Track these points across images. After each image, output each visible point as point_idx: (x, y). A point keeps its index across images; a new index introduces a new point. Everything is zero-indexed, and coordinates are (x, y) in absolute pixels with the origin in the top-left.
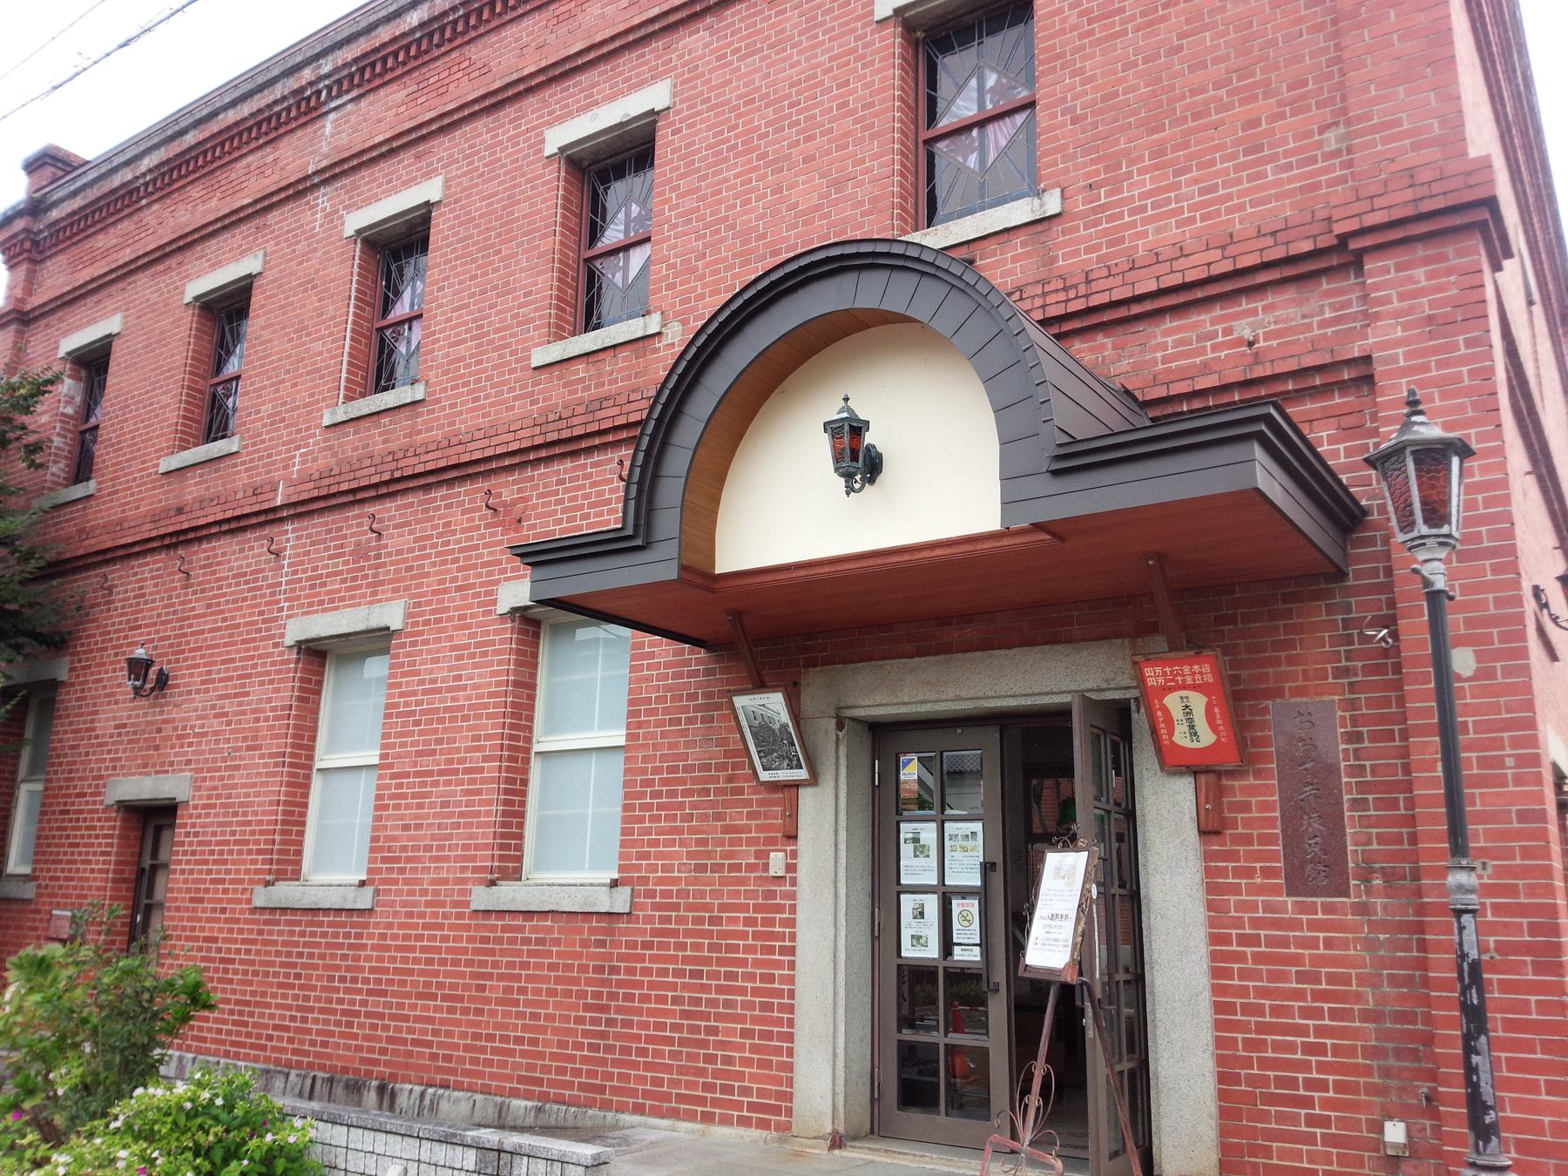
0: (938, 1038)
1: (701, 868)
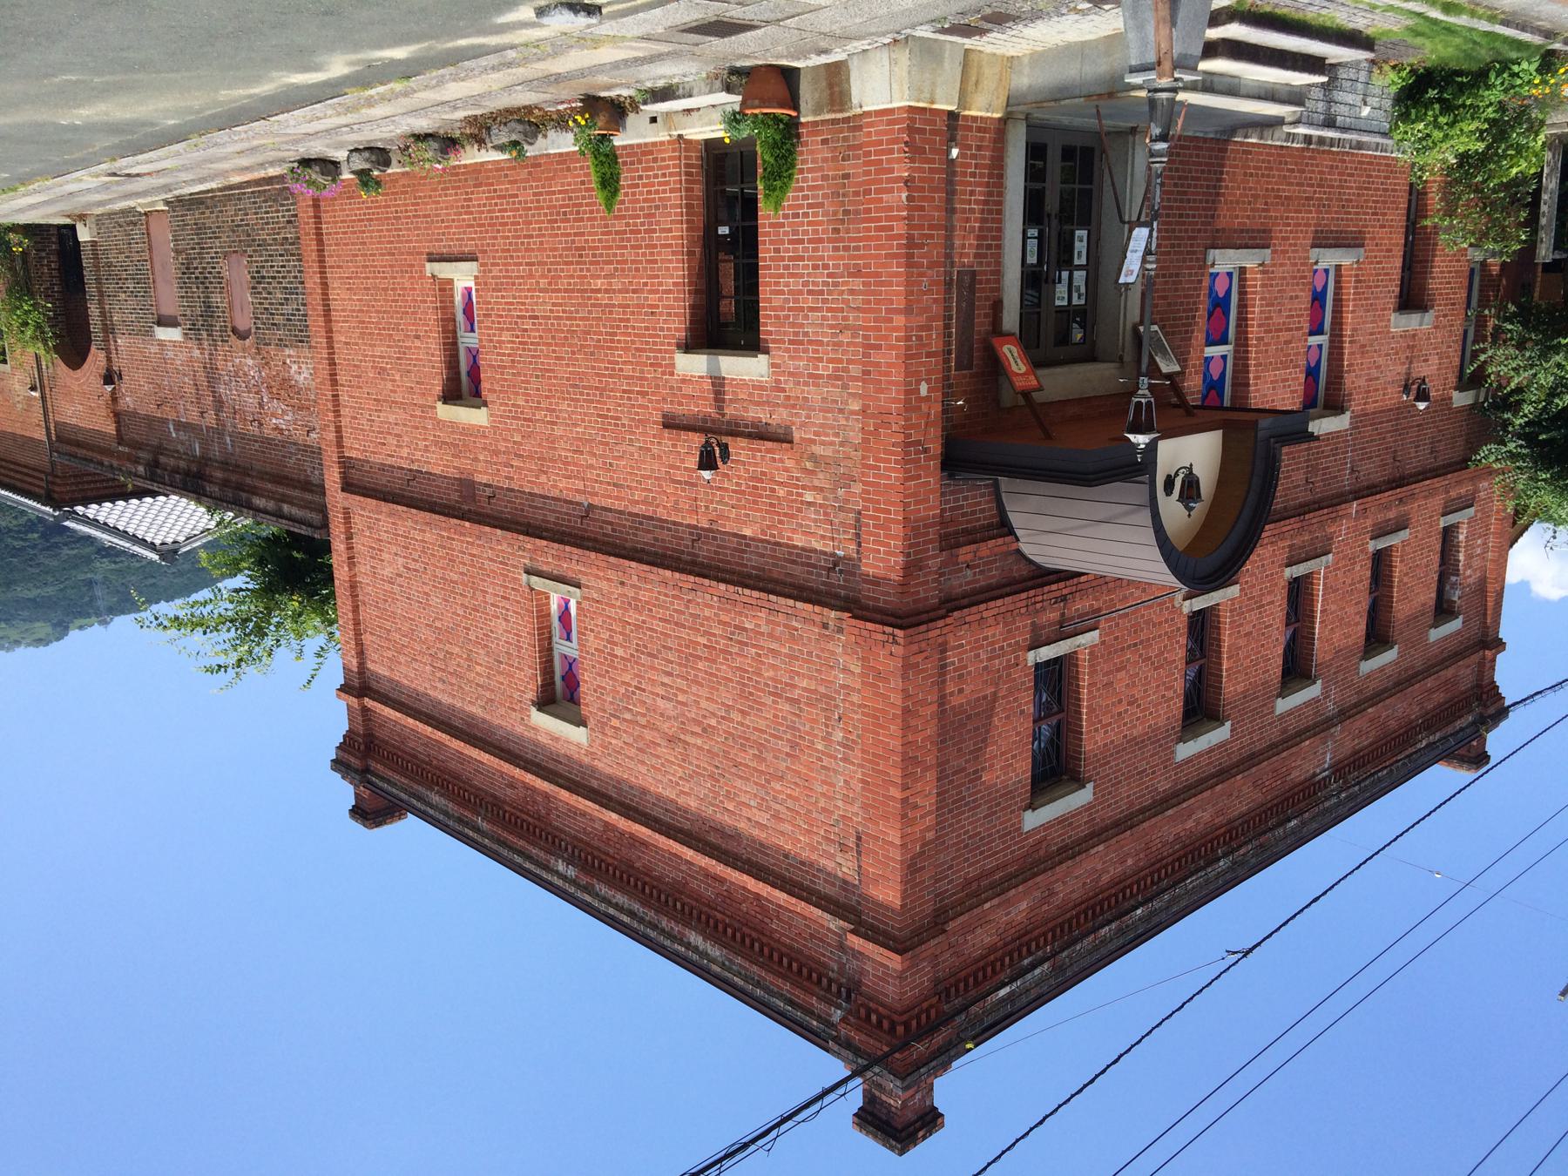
0: (1077, 186)
1: (1177, 275)
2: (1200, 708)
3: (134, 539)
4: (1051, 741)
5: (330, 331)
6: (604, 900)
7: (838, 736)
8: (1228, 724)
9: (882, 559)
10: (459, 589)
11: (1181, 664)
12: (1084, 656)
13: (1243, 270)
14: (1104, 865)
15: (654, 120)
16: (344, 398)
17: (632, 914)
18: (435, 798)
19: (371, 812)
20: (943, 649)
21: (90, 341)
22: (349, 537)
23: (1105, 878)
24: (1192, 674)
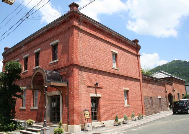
2: (37, 54)
3: (164, 73)
4: (55, 50)
5: (141, 98)
6: (109, 31)
7: (81, 51)
8: (34, 52)
9: (76, 71)
10: (127, 68)
11: (40, 59)
12: (51, 60)
13: (34, 106)
14: (49, 35)
15: (104, 124)
16: (140, 90)
17: (106, 29)
18: (129, 43)
19: (136, 41)
20: (68, 61)
21: (168, 96)
22: (139, 74)
23: (49, 34)
24: (38, 59)
